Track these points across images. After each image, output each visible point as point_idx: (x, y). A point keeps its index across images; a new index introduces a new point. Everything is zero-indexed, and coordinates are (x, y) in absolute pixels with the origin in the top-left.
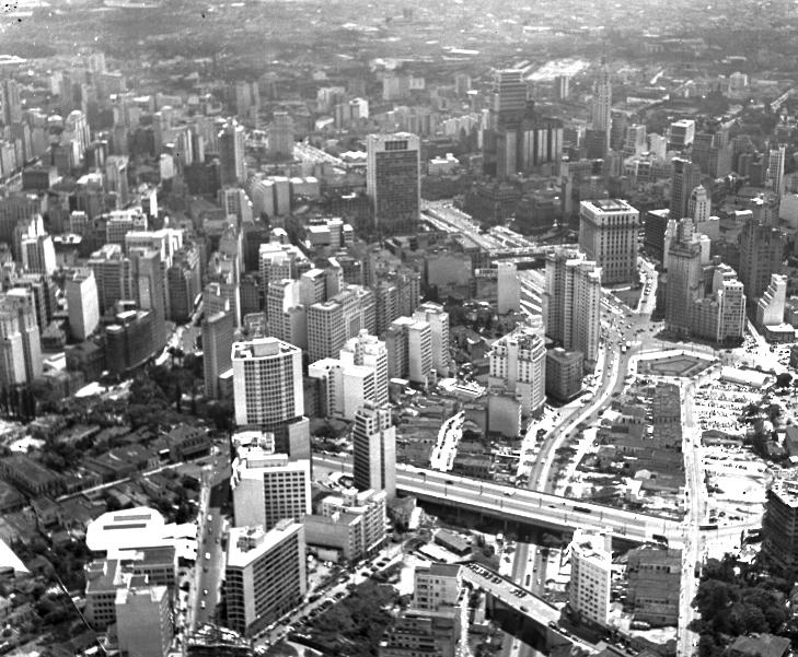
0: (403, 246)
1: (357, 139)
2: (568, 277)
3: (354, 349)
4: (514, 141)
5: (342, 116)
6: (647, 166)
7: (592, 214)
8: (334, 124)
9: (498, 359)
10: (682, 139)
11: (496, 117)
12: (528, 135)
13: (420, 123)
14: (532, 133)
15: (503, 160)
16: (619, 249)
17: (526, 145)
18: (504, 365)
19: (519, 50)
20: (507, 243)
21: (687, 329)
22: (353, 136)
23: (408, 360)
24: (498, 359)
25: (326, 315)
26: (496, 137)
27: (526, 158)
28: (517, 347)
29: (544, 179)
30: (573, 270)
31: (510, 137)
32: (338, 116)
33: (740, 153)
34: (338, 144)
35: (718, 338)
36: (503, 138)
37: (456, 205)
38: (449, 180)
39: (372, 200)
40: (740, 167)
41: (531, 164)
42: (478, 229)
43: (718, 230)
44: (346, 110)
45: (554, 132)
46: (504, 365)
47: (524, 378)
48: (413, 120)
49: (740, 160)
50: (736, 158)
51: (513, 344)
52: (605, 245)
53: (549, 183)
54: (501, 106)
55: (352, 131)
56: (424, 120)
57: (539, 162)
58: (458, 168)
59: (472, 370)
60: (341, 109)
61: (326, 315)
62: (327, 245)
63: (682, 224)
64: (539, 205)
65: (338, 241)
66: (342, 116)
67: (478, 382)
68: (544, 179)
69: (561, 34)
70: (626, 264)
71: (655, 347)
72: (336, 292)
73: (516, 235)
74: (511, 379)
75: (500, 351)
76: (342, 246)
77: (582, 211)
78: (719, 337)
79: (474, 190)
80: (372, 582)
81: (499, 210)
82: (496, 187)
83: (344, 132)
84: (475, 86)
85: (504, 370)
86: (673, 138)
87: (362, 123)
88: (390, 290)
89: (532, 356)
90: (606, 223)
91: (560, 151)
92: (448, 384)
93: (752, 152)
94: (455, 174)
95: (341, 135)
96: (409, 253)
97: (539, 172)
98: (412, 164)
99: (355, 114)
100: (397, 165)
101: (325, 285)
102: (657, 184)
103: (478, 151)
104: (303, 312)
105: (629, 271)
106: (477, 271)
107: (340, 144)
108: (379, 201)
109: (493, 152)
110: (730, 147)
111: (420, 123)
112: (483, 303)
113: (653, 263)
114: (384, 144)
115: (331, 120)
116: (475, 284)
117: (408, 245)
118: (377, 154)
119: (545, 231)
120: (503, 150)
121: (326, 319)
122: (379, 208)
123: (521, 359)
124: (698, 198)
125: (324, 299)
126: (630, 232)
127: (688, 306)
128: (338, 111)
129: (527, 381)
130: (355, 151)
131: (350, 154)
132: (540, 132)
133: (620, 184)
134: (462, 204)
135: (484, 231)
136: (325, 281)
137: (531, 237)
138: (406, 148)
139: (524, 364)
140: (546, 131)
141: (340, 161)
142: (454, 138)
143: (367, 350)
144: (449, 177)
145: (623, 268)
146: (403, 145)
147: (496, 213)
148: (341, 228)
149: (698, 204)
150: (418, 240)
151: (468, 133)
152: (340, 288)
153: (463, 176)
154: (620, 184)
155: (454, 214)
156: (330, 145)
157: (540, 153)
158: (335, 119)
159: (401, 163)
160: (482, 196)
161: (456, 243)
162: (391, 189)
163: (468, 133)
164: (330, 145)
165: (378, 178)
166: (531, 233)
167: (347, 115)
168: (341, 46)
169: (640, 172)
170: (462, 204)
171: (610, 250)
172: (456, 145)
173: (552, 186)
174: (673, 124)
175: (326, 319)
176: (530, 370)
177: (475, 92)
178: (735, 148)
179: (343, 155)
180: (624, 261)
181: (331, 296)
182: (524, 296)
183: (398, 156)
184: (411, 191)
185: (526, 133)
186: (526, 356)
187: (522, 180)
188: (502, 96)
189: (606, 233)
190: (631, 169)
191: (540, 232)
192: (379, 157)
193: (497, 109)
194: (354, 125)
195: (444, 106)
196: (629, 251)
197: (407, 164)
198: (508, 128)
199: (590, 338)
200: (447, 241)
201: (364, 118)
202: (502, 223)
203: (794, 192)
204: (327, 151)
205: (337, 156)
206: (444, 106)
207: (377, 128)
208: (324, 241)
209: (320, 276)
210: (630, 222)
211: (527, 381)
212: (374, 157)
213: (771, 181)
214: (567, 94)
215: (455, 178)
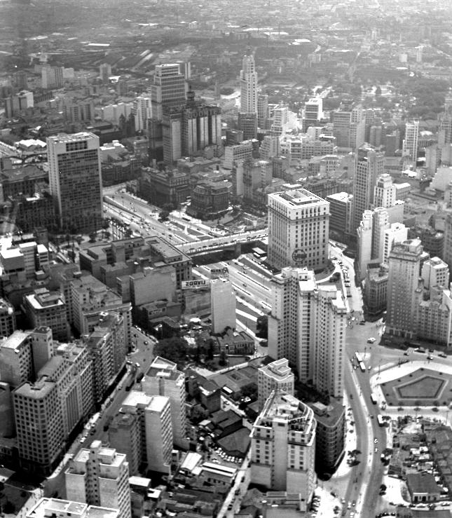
0: (100, 258)
2: (302, 304)
4: (179, 128)
5: (12, 107)
6: (299, 145)
7: (285, 210)
9: (262, 443)
10: (316, 116)
12: (192, 123)
13: (82, 110)
14: (194, 120)
15: (170, 146)
16: (312, 240)
17: (190, 132)
18: (270, 450)
19: (140, 42)
20: (189, 230)
21: (411, 333)
22: (22, 125)
23: (145, 450)
24: (262, 443)
25: (38, 404)
26: (160, 126)
27: (190, 143)
28: (287, 427)
30: (309, 295)
31: (175, 126)
32: (9, 109)
34: (11, 132)
36: (168, 127)
37: (129, 189)
38: (120, 167)
40: (371, 137)
42: (157, 216)
43: (403, 212)
44: (16, 101)
45: (213, 119)
47: (297, 465)
48: (76, 109)
49: (372, 132)
50: (368, 129)
51: (281, 425)
55: (22, 121)
57: (202, 145)
58: (126, 154)
60: (11, 101)
61: (38, 404)
62: (21, 270)
63: (376, 213)
64: (214, 191)
65: (33, 263)
66: (12, 107)
67: (224, 450)
69: (168, 28)
70: (318, 253)
71: (387, 361)
72: (45, 361)
73: (194, 221)
76: (37, 269)
77: (270, 203)
79: (147, 177)
81: (174, 196)
85: (270, 455)
86: (308, 115)
87: (30, 113)
88: (105, 338)
90: (300, 216)
91: (219, 134)
92: (191, 462)
93: (381, 124)
94: (124, 160)
95: (14, 123)
96: (108, 268)
99: (22, 105)
100: (79, 164)
102: (311, 161)
104: (8, 390)
105: (321, 260)
106: (184, 284)
108: (62, 201)
109: (160, 138)
110: (364, 121)
111: (82, 110)
112: (196, 320)
113: (341, 248)
118: (59, 155)
119: (223, 215)
120: (169, 138)
121: (39, 409)
123: (293, 443)
124: (386, 185)
127: (413, 310)
128: (8, 103)
131: (23, 142)
132: (202, 119)
133: (280, 164)
134: (135, 189)
137: (210, 222)
140: (206, 118)
141: (14, 148)
143: (103, 470)
144: (118, 164)
145: (316, 257)
148: (35, 249)
149: (385, 192)
150: (115, 250)
151: (127, 118)
152: (50, 353)
154: (280, 164)
157: (202, 139)
158: (6, 110)
159: (83, 163)
160: (156, 182)
161: (153, 249)
163: (127, 118)
165: (61, 178)
167: (16, 106)
168: (153, 15)
169: (293, 151)
170: (135, 189)
172: (117, 130)
174: (306, 103)
175: (39, 409)
177: (117, 78)
180: (317, 250)
181: (40, 367)
182: (240, 306)
183: (79, 156)
185: (190, 121)
186: (298, 439)
187: (191, 165)
188: (162, 89)
189: (300, 226)
190: (285, 148)
191: (218, 217)
192: (61, 159)
193: (159, 99)
195: (95, 91)
196: (321, 241)
197: (88, 163)
198: (173, 118)
199: (337, 373)
200: (144, 248)
201: (31, 108)
202: (178, 208)
203: (449, 166)
205: (12, 145)
206: (95, 91)
207: (44, 116)
209: (25, 342)
210: (322, 213)
212: (56, 159)
214: (189, 76)
215: (125, 164)
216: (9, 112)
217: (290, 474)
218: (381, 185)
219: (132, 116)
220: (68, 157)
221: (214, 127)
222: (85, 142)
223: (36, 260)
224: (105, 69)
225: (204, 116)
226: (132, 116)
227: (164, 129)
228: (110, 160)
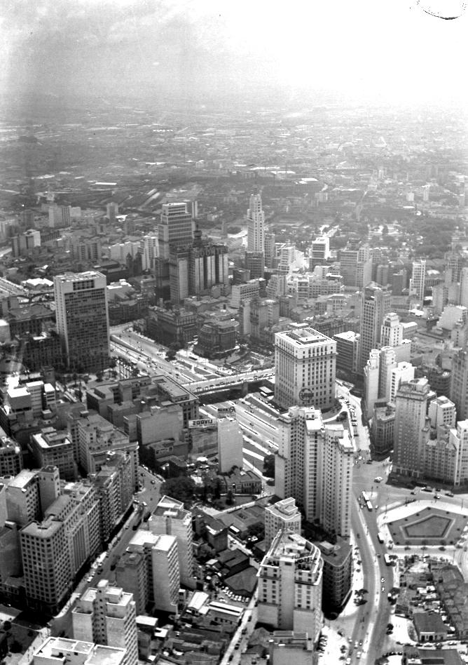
0: (107, 397)
2: (309, 443)
3: (92, 609)
4: (186, 267)
5: (19, 246)
6: (306, 283)
8: (13, 253)
9: (269, 582)
10: (323, 255)
11: (166, 246)
12: (199, 262)
13: (89, 249)
14: (201, 259)
15: (177, 286)
17: (197, 271)
18: (277, 590)
19: (147, 180)
20: (196, 369)
21: (418, 472)
23: (152, 590)
24: (269, 582)
25: (45, 543)
28: (294, 566)
29: (215, 300)
30: (316, 435)
31: (182, 264)
32: (16, 247)
33: (377, 265)
34: (18, 271)
35: (455, 481)
36: (175, 266)
37: (136, 329)
38: (127, 306)
39: (64, 341)
40: (378, 276)
42: (164, 355)
44: (23, 240)
45: (220, 258)
47: (304, 605)
48: (83, 248)
49: (379, 270)
50: (375, 268)
52: (306, 377)
54: (170, 236)
55: (30, 260)
57: (209, 284)
58: (132, 293)
59: (220, 570)
61: (45, 543)
62: (28, 409)
63: (383, 353)
64: (221, 330)
65: (40, 402)
67: (231, 589)
68: (215, 300)
69: (175, 167)
70: (325, 392)
72: (52, 501)
73: (201, 360)
75: (270, 573)
76: (44, 409)
77: (277, 342)
78: (456, 480)
79: (154, 316)
82: (177, 314)
85: (277, 595)
87: (37, 252)
88: (112, 477)
89: (313, 578)
90: (307, 355)
92: (198, 601)
93: (387, 263)
94: (131, 299)
95: (20, 262)
96: (115, 407)
97: (210, 294)
100: (86, 303)
104: (15, 529)
105: (328, 399)
106: (191, 423)
107: (20, 271)
109: (167, 277)
110: (371, 260)
111: (89, 249)
112: (203, 459)
113: (348, 387)
115: (10, 250)
117: (112, 396)
118: (66, 294)
119: (229, 354)
120: (176, 277)
121: (46, 548)
123: (300, 582)
128: (15, 242)
131: (30, 281)
132: (209, 258)
133: (287, 303)
134: (142, 328)
137: (217, 361)
140: (213, 257)
141: (21, 287)
142: (121, 263)
143: (110, 610)
145: (323, 396)
147: (178, 338)
148: (42, 388)
152: (57, 492)
154: (287, 303)
155: (136, 338)
156: (10, 273)
157: (209, 278)
159: (90, 301)
161: (160, 388)
162: (81, 327)
164: (10, 273)
166: (217, 357)
167: (23, 245)
168: (160, 154)
172: (124, 269)
173: (225, 308)
175: (46, 548)
177: (124, 217)
178: (373, 261)
180: (324, 389)
181: (48, 506)
182: (247, 445)
183: (87, 295)
185: (197, 260)
186: (305, 578)
187: (198, 304)
188: (170, 228)
189: (307, 366)
191: (225, 356)
192: (68, 298)
193: (166, 239)
194: (31, 254)
195: (102, 230)
196: (328, 380)
197: (95, 302)
200: (151, 387)
201: (38, 247)
202: (185, 347)
204: (8, 279)
205: (19, 284)
206: (102, 230)
209: (32, 481)
210: (328, 352)
211: (308, 607)
213: (415, 290)
215: (132, 303)
216: (16, 251)
217: (297, 613)
218: (388, 325)
220: (75, 296)
221: (221, 266)
222: (92, 281)
223: (43, 400)
225: (211, 255)
226: (139, 255)
227: (171, 269)
228: (117, 299)
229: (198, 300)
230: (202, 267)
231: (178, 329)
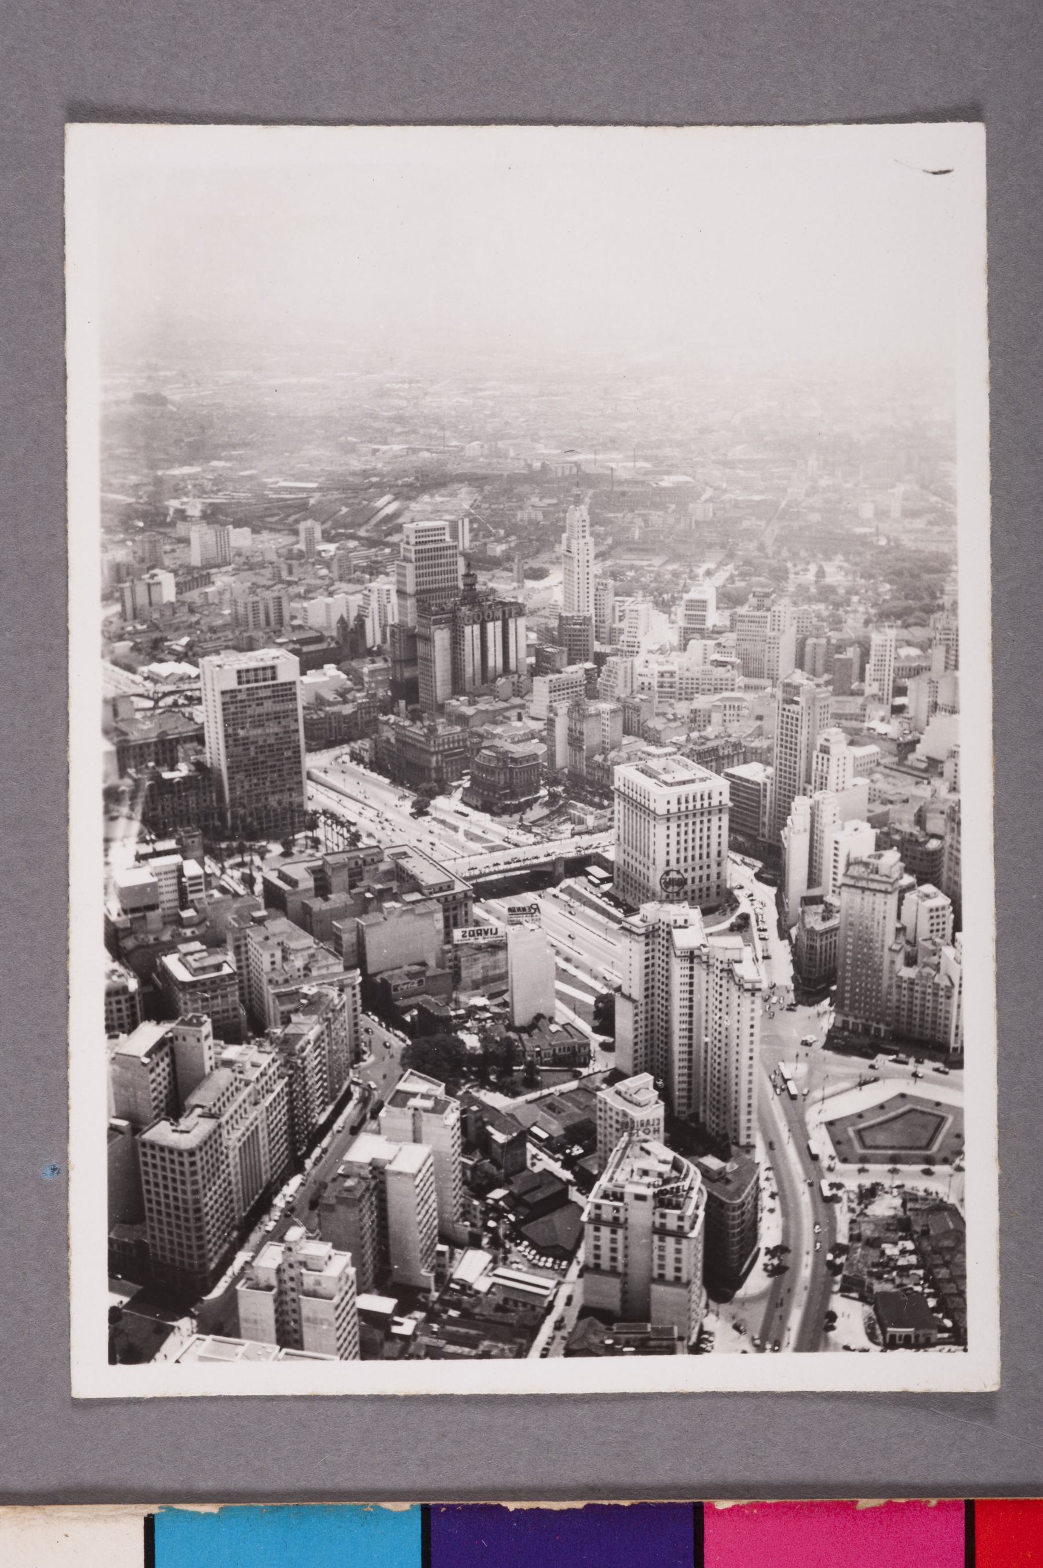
0: (302, 886)
1: (164, 639)
2: (678, 970)
3: (274, 1282)
10: (703, 619)
11: (411, 603)
12: (471, 632)
13: (267, 607)
14: (477, 628)
15: (430, 675)
18: (620, 1246)
21: (882, 1027)
22: (156, 635)
27: (469, 670)
28: (650, 1203)
29: (503, 705)
31: (441, 637)
34: (132, 649)
36: (428, 640)
38: (338, 715)
40: (808, 658)
41: (478, 682)
44: (141, 590)
46: (620, 1246)
47: (670, 1274)
49: (808, 649)
50: (801, 645)
52: (673, 848)
53: (513, 714)
55: (154, 627)
56: (271, 605)
57: (490, 674)
61: (186, 1160)
62: (153, 907)
65: (175, 896)
67: (533, 1245)
68: (503, 705)
69: (426, 455)
70: (708, 876)
71: (839, 1079)
72: (199, 1079)
74: (637, 1272)
76: (184, 906)
79: (389, 734)
80: (134, 665)
81: (439, 769)
82: (432, 730)
83: (139, 627)
84: (328, 538)
86: (689, 618)
87: (168, 612)
90: (674, 808)
92: (472, 1267)
94: (345, 702)
95: (137, 632)
96: (318, 905)
97: (493, 693)
98: (792, 1336)
100: (260, 710)
101: (173, 1064)
103: (372, 654)
104: (128, 1137)
105: (714, 890)
107: (136, 648)
111: (267, 607)
114: (235, 676)
116: (456, 958)
118: (223, 693)
119: (529, 804)
120: (429, 661)
122: (232, 789)
123: (662, 1232)
124: (834, 750)
125: (174, 1108)
126: (715, 819)
127: (885, 983)
129: (678, 1279)
130: (161, 661)
132: (490, 626)
133: (637, 710)
134: (366, 757)
135: (420, 811)
136: (172, 1054)
137: (506, 818)
138: (274, 678)
139: (670, 1241)
144: (335, 709)
146: (269, 673)
147: (434, 775)
148: (180, 870)
151: (352, 624)
152: (208, 1064)
153: (360, 707)
154: (637, 710)
157: (491, 663)
158: (123, 606)
159: (269, 706)
160: (405, 743)
163: (352, 624)
167: (142, 599)
171: (682, 855)
173: (520, 719)
175: (187, 1168)
176: (684, 1256)
179: (144, 669)
180: (705, 872)
183: (262, 693)
184: (288, 754)
185: (468, 630)
186: (672, 1223)
187: (470, 711)
189: (673, 826)
191: (521, 808)
193: (410, 588)
197: (279, 707)
200: (383, 867)
208: (147, 901)
209: (161, 1044)
210: (715, 802)
211: (678, 1279)
214: (467, 544)
215: (348, 709)
219: (360, 620)
223: (182, 891)
224: (310, 532)
226: (360, 620)
227: (421, 647)
229: (472, 703)
230: (477, 642)
231: (434, 759)
